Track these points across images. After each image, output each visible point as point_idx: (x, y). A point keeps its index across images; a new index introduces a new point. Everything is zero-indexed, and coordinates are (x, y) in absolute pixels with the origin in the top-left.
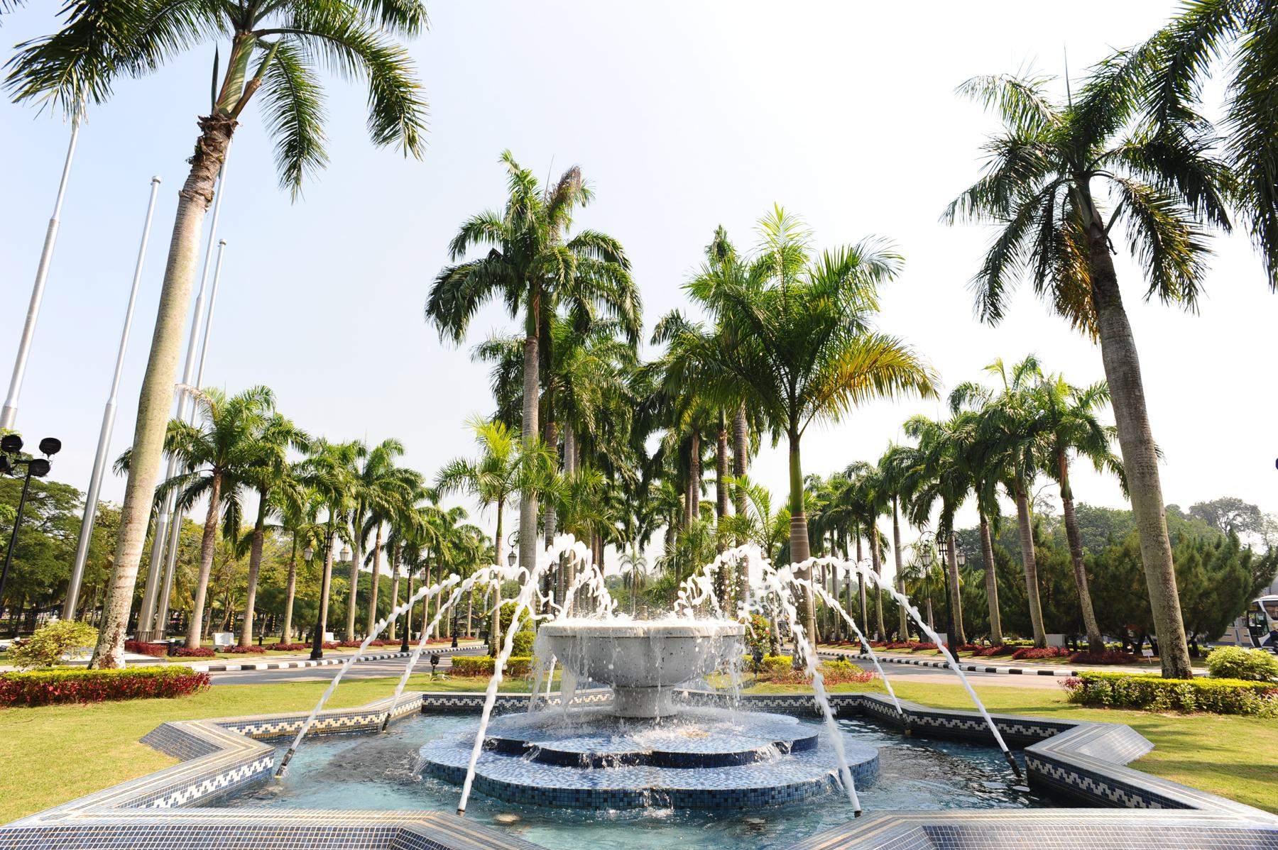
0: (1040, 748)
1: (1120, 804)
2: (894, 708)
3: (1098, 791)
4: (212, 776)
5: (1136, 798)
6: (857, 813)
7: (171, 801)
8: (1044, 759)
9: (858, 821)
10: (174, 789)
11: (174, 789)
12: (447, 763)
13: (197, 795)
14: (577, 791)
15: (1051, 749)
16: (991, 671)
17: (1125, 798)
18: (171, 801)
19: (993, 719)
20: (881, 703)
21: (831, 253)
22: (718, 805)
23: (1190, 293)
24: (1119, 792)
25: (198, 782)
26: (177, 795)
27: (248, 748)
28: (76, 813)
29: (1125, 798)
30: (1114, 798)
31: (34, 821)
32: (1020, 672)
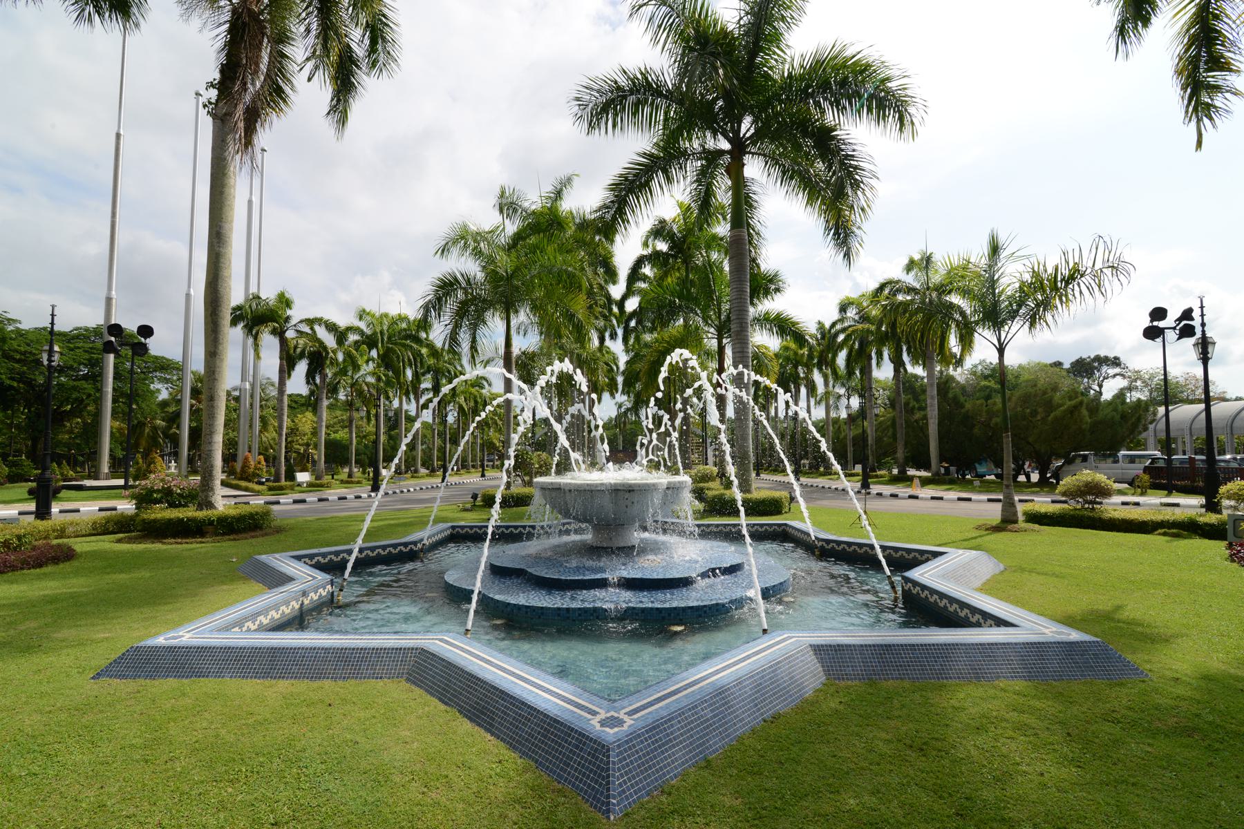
0: (916, 574)
1: (978, 625)
2: (809, 535)
3: (962, 614)
4: (276, 607)
5: (990, 622)
6: (765, 631)
7: (244, 629)
8: (915, 583)
9: (766, 637)
10: (259, 614)
11: (259, 614)
12: (172, 683)
13: (265, 621)
14: (559, 609)
15: (922, 575)
16: (894, 496)
17: (982, 621)
18: (244, 629)
19: (882, 547)
20: (799, 530)
21: (838, 44)
22: (663, 618)
23: (914, 134)
24: (977, 616)
25: (287, 603)
26: (249, 624)
27: (314, 578)
28: (188, 635)
29: (982, 621)
30: (974, 620)
31: (160, 641)
32: (916, 498)
